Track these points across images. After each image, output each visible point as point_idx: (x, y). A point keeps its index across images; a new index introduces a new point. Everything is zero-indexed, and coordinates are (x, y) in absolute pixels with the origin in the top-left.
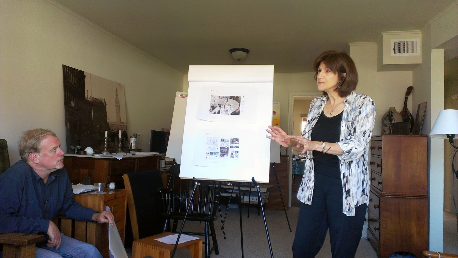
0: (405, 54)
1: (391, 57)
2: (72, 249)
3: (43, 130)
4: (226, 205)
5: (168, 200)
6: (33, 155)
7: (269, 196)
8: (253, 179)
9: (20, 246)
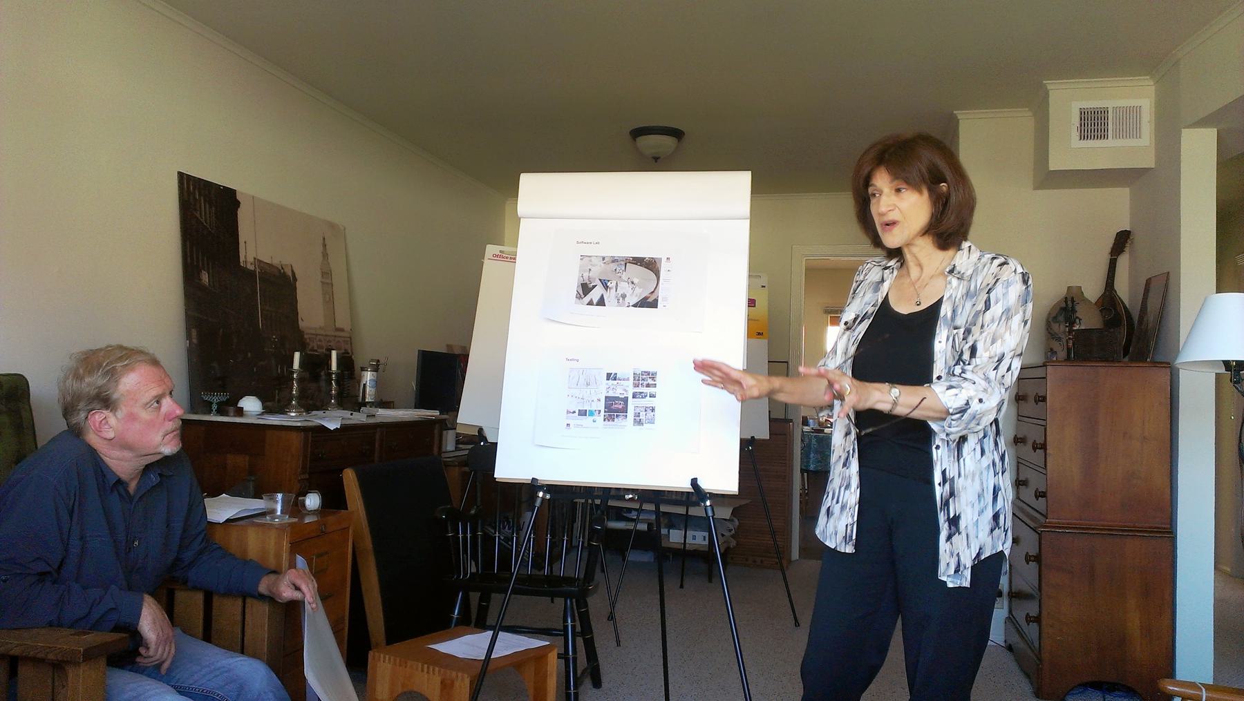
0: (1110, 143)
3: (126, 349)
4: (622, 552)
5: (465, 538)
6: (98, 417)
9: (67, 662)
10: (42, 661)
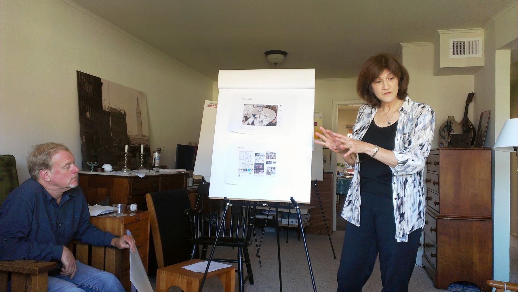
1: (449, 59)
3: (55, 144)
4: (262, 228)
5: (197, 222)
6: (43, 172)
7: (310, 218)
10: (21, 274)
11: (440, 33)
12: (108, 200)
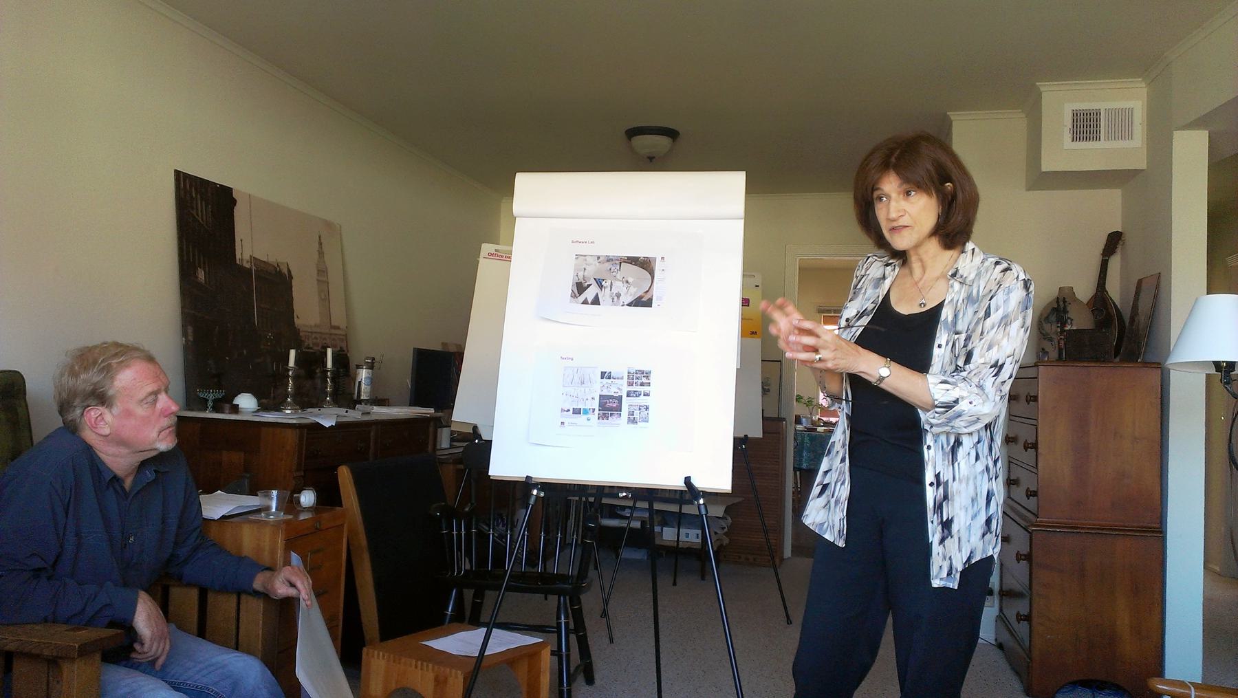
1: (1064, 152)
2: (202, 666)
3: (121, 345)
4: (616, 549)
5: (459, 535)
6: (93, 413)
8: (688, 481)
10: (38, 656)
11: (1042, 89)
12: (246, 482)
